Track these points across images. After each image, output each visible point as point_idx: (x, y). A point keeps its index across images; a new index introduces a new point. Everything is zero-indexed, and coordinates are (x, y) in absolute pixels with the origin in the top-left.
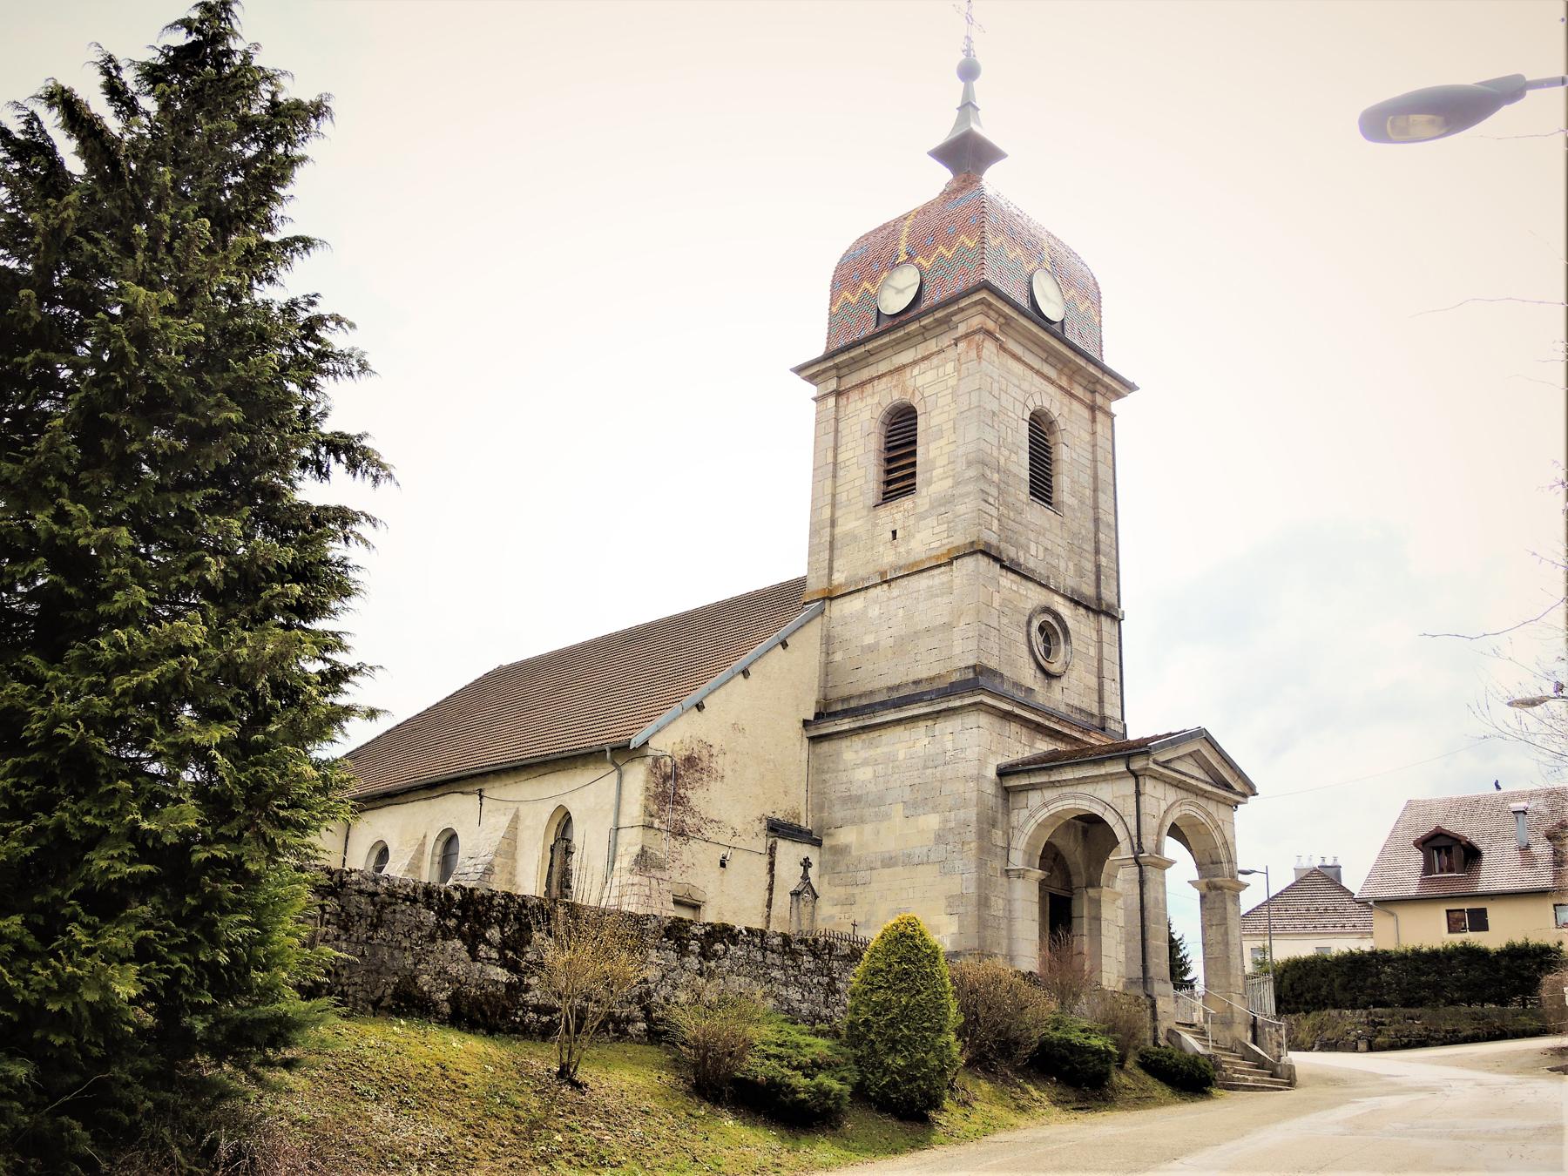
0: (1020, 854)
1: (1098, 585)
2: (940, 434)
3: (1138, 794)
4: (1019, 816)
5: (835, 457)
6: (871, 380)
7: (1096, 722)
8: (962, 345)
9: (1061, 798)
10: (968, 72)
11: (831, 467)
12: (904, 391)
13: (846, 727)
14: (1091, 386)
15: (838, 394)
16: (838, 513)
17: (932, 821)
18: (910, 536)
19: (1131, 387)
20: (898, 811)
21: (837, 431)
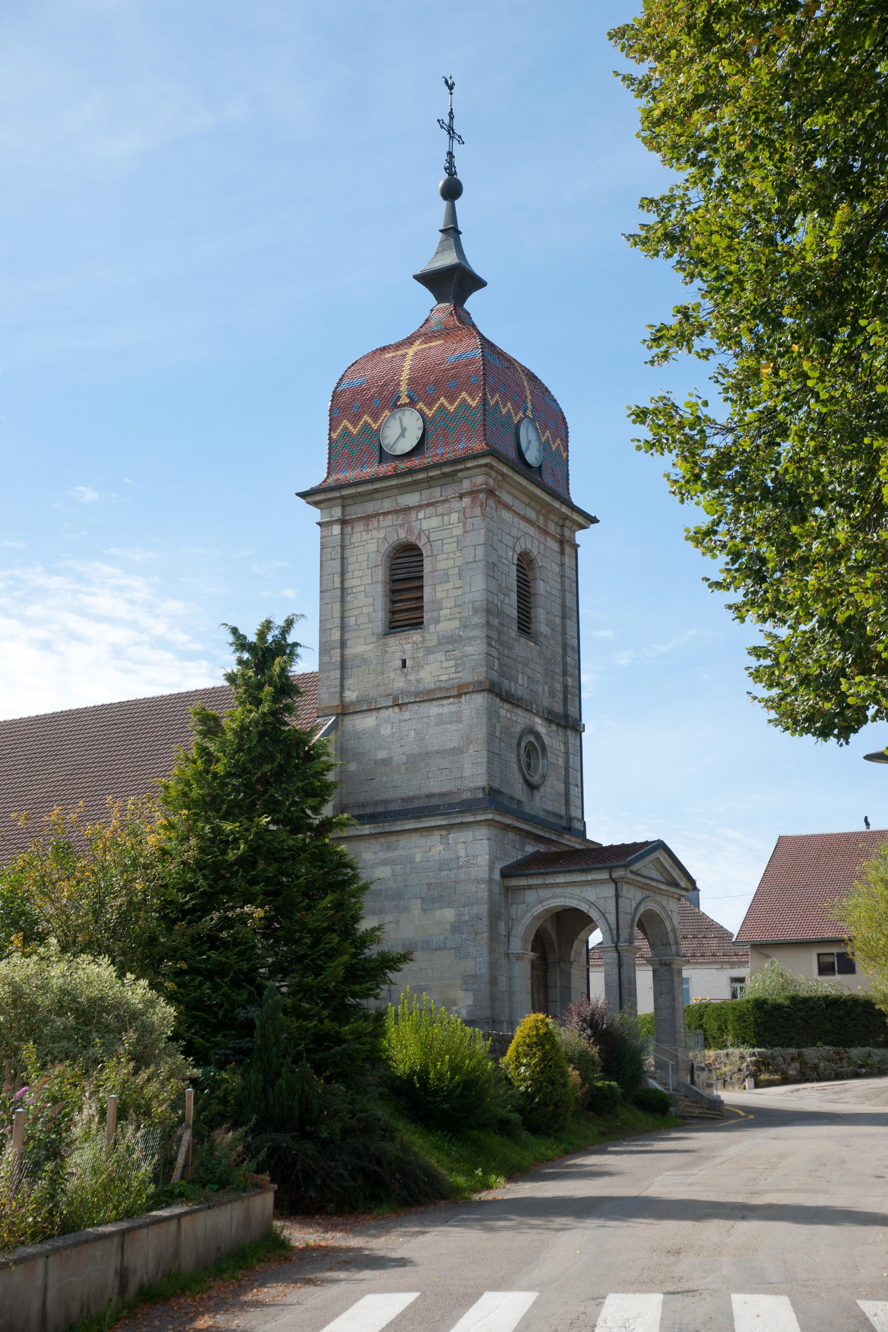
0: (519, 940)
1: (565, 704)
2: (447, 578)
3: (617, 896)
4: (516, 910)
5: (342, 582)
6: (377, 515)
7: (564, 823)
8: (466, 501)
9: (553, 897)
10: (452, 191)
11: (339, 592)
12: (410, 531)
13: (367, 832)
14: (561, 522)
15: (343, 522)
16: (348, 636)
17: (448, 915)
18: (418, 667)
19: (594, 520)
20: (416, 906)
21: (343, 558)
